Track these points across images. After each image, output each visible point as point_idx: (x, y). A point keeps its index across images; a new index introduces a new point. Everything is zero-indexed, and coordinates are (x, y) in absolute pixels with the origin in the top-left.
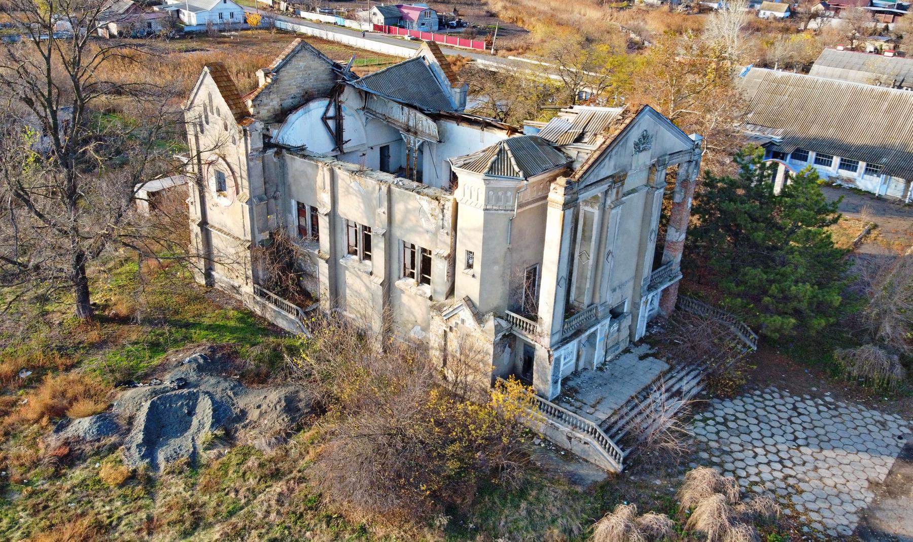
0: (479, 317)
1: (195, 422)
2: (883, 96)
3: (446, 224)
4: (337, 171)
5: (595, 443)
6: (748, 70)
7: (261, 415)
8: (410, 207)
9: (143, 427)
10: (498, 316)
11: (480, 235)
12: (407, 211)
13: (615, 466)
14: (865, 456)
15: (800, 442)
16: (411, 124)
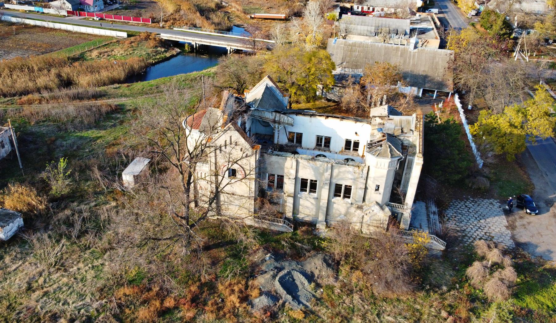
0: (382, 208)
1: (298, 283)
2: (397, 48)
3: (363, 176)
4: (300, 160)
5: (435, 242)
6: (336, 40)
7: (320, 271)
8: (341, 170)
9: (285, 292)
10: (388, 205)
11: (385, 179)
12: (340, 172)
13: (443, 248)
14: (497, 218)
15: (478, 219)
16: (276, 119)
